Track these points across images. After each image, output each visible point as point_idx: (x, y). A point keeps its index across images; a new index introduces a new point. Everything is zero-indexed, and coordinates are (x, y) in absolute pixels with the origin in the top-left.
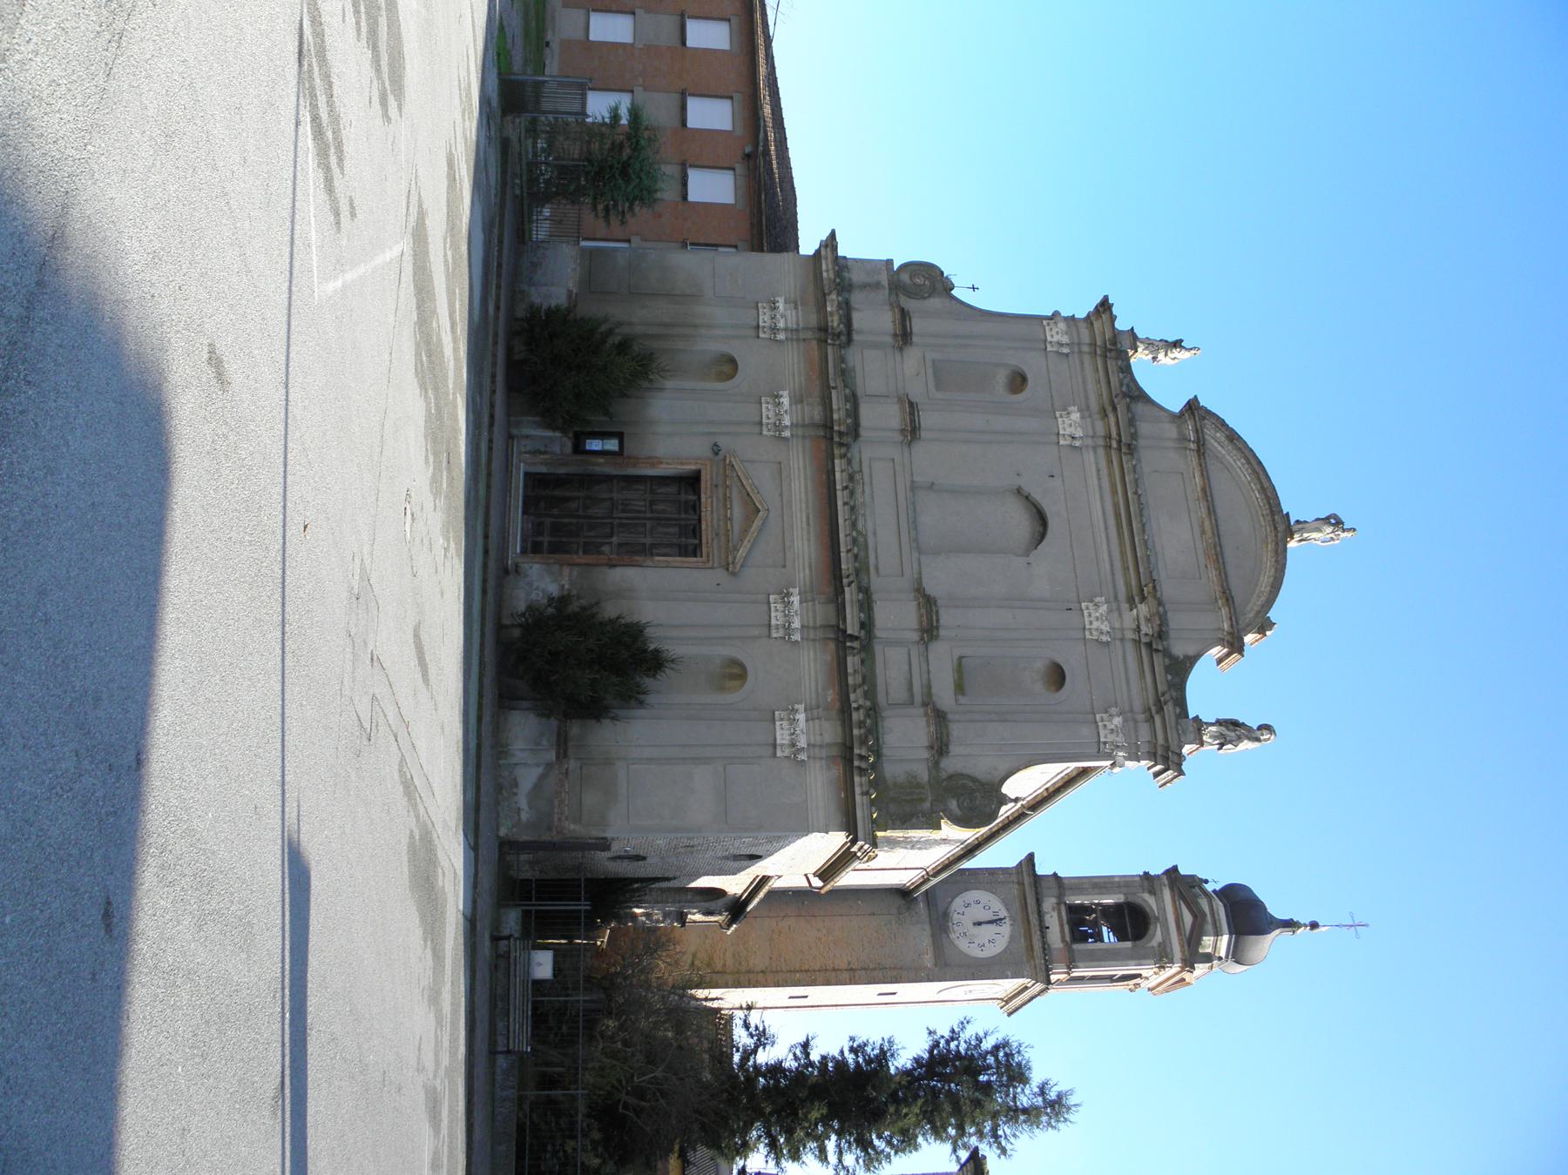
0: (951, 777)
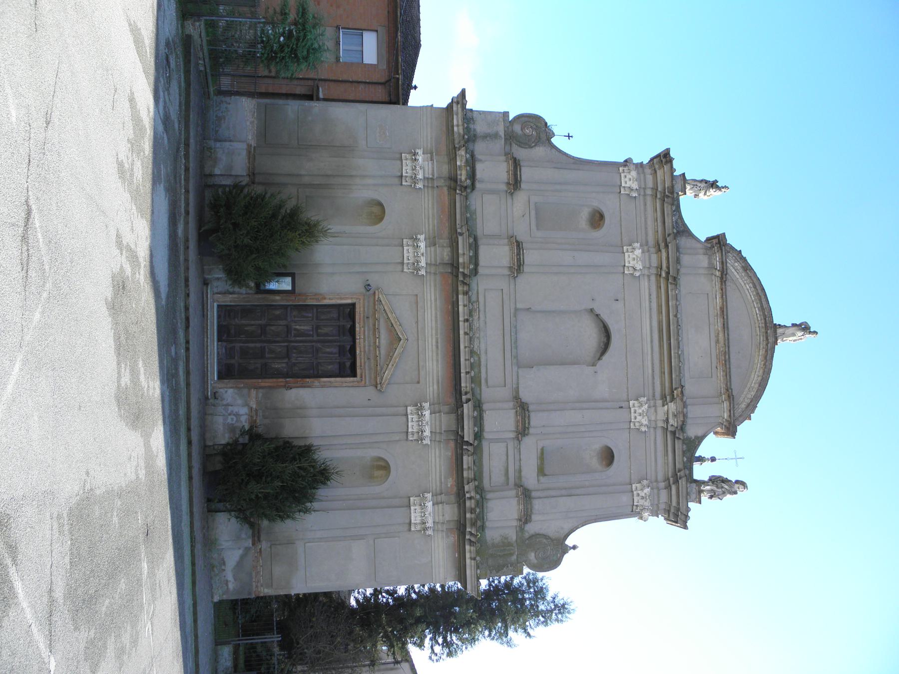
0: (531, 537)
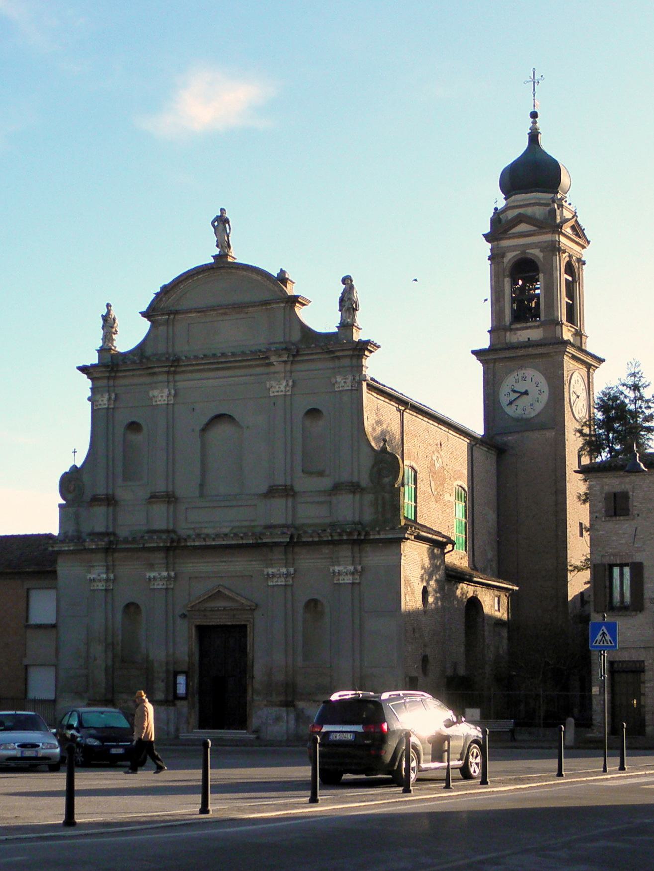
0: (371, 481)
